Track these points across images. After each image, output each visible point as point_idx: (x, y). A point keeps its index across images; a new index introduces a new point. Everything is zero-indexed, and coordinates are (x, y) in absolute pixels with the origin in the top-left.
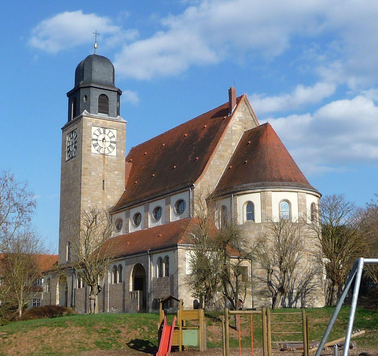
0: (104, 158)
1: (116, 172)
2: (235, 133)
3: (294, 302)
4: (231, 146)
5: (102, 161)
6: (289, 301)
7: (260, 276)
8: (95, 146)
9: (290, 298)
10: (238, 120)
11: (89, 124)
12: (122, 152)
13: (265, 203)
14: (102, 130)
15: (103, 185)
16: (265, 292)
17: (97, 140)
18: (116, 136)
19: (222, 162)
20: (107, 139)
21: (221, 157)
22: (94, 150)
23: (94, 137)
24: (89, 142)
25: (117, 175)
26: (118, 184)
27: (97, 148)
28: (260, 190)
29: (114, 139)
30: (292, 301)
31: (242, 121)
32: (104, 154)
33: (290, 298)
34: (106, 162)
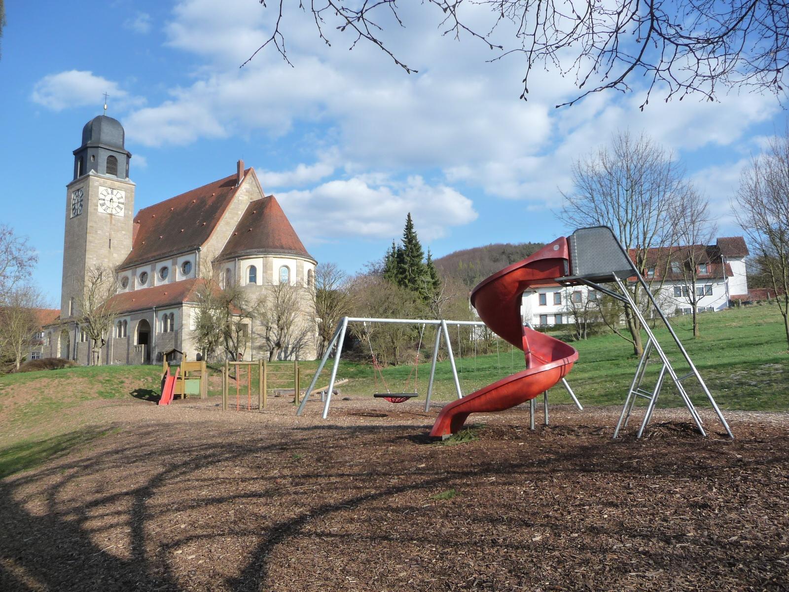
0: (111, 217)
1: (123, 232)
2: (241, 202)
3: (289, 356)
4: (237, 214)
5: (109, 220)
6: (285, 354)
7: (259, 333)
8: (102, 205)
9: (286, 352)
10: (245, 191)
11: (96, 184)
12: (130, 213)
13: (267, 268)
14: (110, 191)
15: (110, 244)
16: (263, 346)
17: (104, 200)
18: (124, 197)
19: (228, 228)
20: (115, 199)
21: (228, 223)
22: (100, 209)
23: (101, 197)
24: (95, 201)
25: (125, 235)
26: (125, 243)
27: (104, 207)
28: (262, 256)
29: (122, 201)
30: (287, 355)
31: (249, 193)
32: (111, 214)
33: (286, 352)
34: (113, 222)
